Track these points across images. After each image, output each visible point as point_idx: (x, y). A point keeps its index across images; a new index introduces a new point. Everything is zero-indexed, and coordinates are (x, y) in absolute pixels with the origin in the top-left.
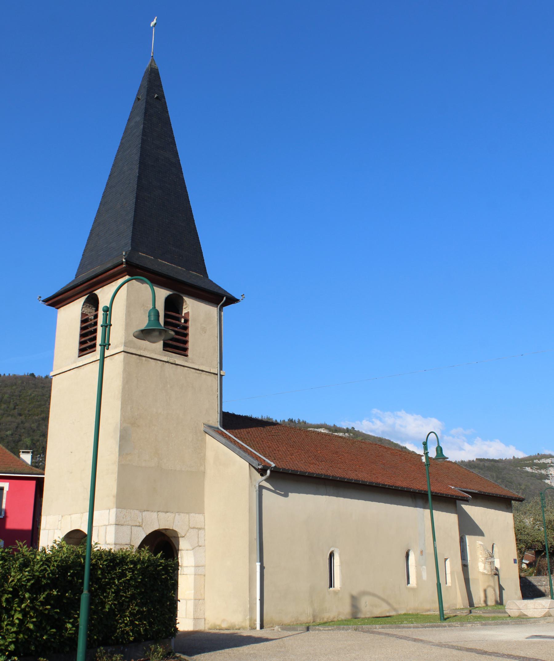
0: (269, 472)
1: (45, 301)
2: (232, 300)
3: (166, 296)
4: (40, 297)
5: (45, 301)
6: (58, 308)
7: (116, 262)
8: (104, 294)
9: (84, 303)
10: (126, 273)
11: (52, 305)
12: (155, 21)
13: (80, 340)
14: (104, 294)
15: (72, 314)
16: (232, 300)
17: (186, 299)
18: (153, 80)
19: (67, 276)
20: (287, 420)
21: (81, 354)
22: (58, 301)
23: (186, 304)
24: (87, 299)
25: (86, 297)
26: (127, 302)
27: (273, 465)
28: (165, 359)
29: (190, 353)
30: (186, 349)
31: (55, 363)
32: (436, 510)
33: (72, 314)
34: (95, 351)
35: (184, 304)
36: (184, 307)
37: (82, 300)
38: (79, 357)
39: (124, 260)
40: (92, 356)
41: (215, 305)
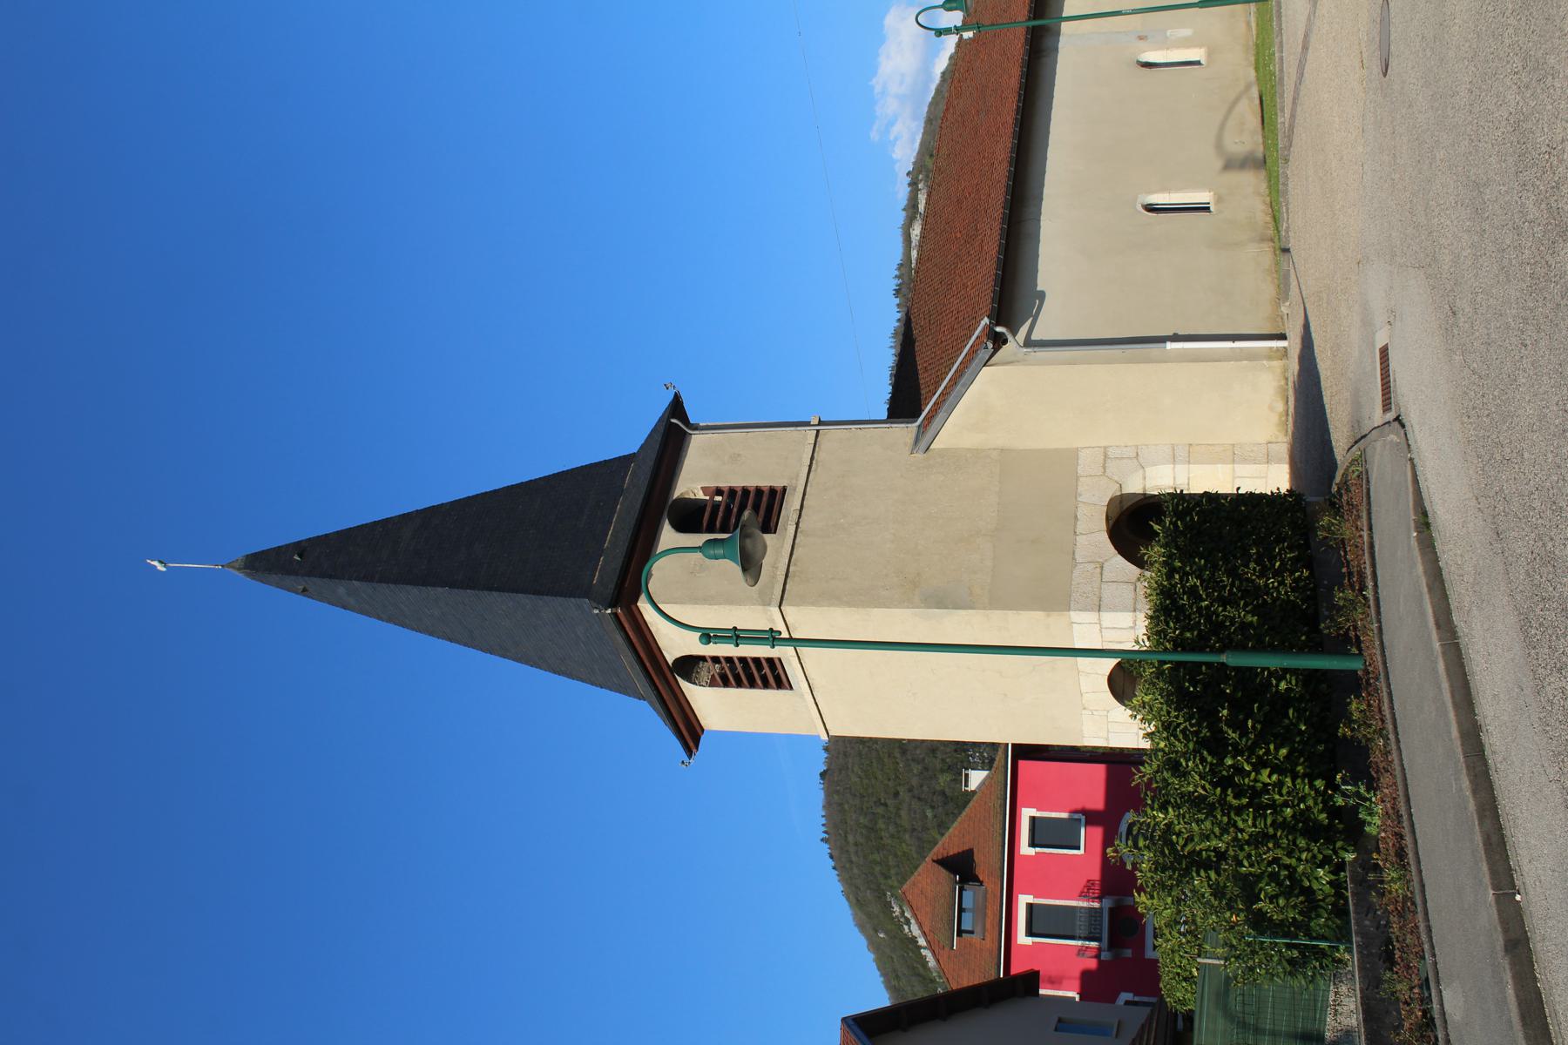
0: (998, 329)
1: (690, 753)
5: (690, 753)
12: (155, 563)
14: (675, 644)
15: (712, 705)
17: (676, 494)
18: (269, 564)
19: (641, 717)
20: (897, 301)
22: (689, 731)
26: (689, 600)
27: (986, 320)
29: (778, 483)
30: (773, 491)
32: (1062, 10)
33: (712, 705)
37: (685, 685)
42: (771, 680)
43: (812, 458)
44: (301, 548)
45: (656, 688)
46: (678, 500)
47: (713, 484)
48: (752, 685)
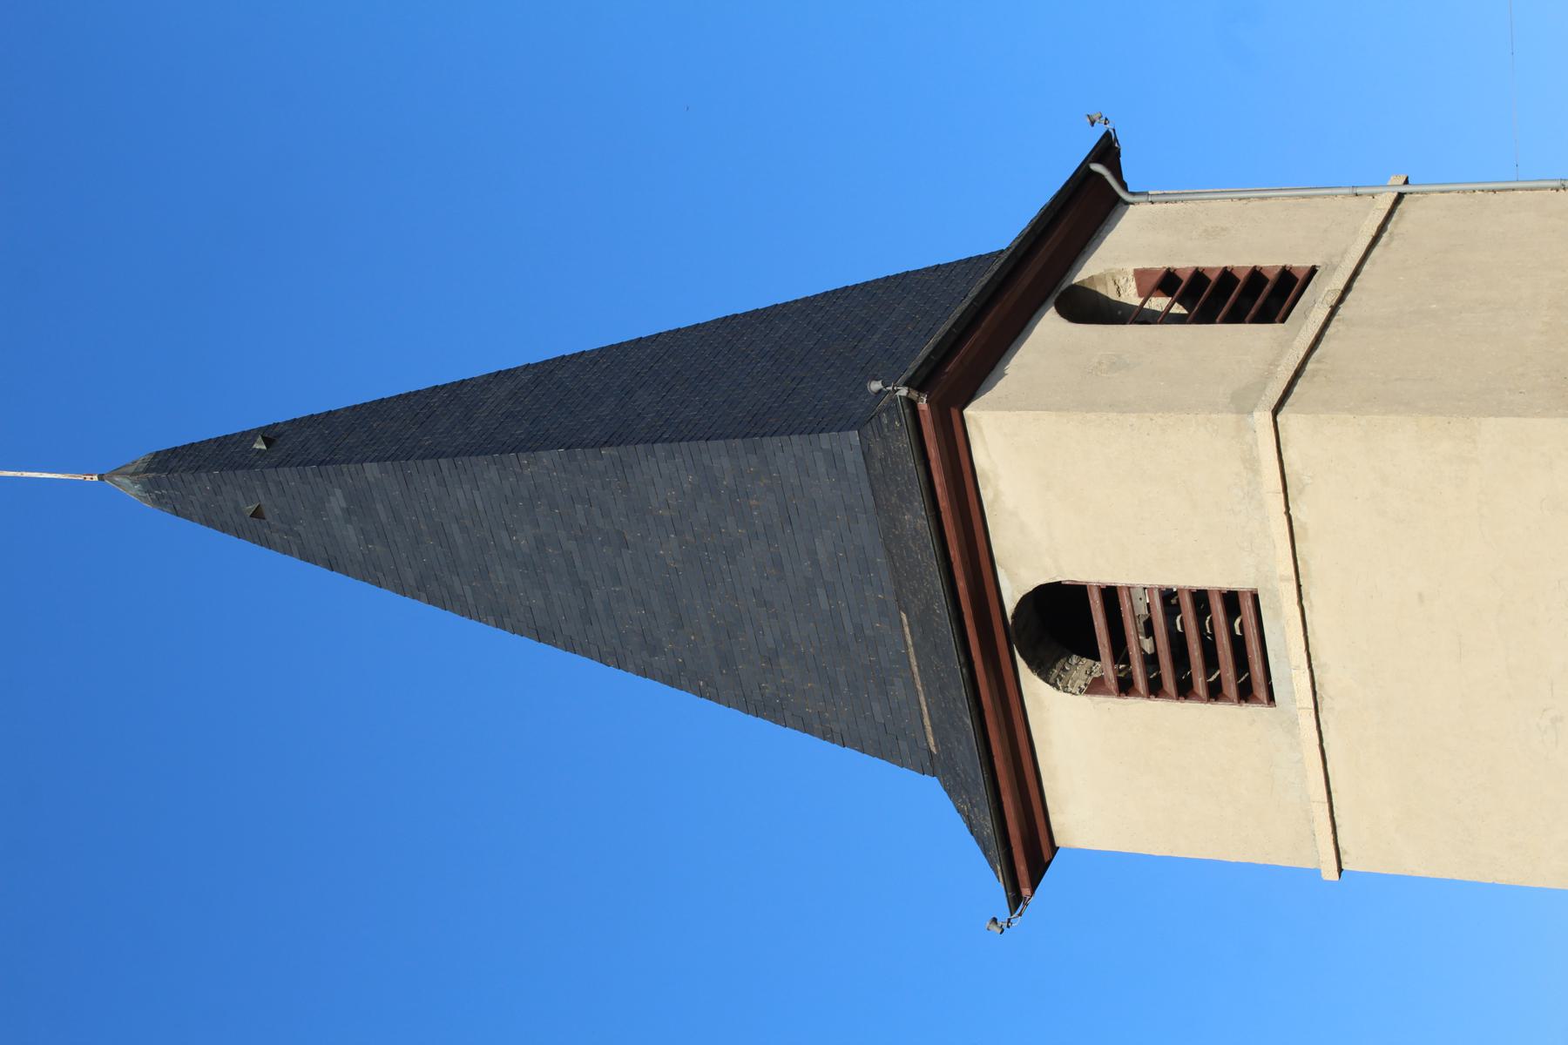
1: (1016, 901)
2: (1107, 150)
3: (1057, 316)
4: (995, 920)
5: (1016, 901)
6: (1054, 849)
7: (902, 424)
8: (1031, 552)
9: (1046, 680)
10: (954, 412)
11: (1038, 868)
13: (1201, 700)
14: (1031, 552)
16: (1107, 150)
17: (1081, 276)
18: (204, 476)
19: (919, 820)
21: (1261, 693)
22: (1021, 843)
23: (1101, 279)
24: (1030, 664)
25: (1022, 664)
26: (1074, 470)
28: (1321, 314)
29: (1299, 262)
30: (1286, 275)
31: (1282, 858)
34: (1255, 597)
35: (1101, 290)
36: (1113, 296)
37: (1030, 682)
38: (1271, 698)
39: (903, 392)
40: (1278, 613)
41: (1120, 207)
42: (1217, 607)
43: (1382, 229)
44: (271, 435)
45: (969, 663)
46: (1075, 286)
47: (1160, 264)
48: (1185, 690)
